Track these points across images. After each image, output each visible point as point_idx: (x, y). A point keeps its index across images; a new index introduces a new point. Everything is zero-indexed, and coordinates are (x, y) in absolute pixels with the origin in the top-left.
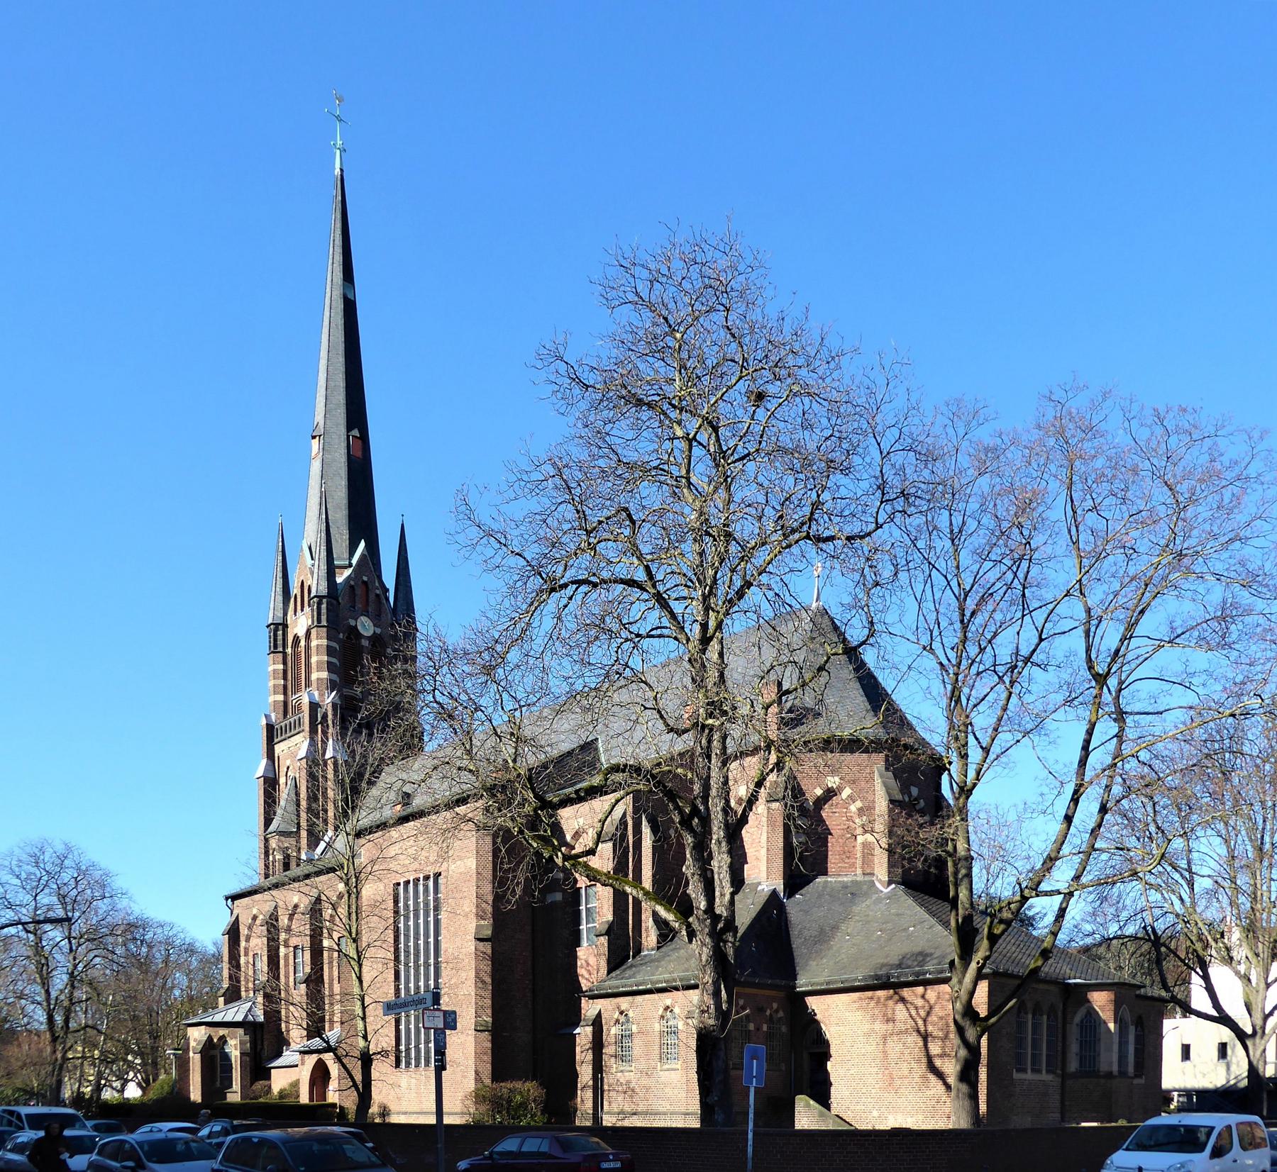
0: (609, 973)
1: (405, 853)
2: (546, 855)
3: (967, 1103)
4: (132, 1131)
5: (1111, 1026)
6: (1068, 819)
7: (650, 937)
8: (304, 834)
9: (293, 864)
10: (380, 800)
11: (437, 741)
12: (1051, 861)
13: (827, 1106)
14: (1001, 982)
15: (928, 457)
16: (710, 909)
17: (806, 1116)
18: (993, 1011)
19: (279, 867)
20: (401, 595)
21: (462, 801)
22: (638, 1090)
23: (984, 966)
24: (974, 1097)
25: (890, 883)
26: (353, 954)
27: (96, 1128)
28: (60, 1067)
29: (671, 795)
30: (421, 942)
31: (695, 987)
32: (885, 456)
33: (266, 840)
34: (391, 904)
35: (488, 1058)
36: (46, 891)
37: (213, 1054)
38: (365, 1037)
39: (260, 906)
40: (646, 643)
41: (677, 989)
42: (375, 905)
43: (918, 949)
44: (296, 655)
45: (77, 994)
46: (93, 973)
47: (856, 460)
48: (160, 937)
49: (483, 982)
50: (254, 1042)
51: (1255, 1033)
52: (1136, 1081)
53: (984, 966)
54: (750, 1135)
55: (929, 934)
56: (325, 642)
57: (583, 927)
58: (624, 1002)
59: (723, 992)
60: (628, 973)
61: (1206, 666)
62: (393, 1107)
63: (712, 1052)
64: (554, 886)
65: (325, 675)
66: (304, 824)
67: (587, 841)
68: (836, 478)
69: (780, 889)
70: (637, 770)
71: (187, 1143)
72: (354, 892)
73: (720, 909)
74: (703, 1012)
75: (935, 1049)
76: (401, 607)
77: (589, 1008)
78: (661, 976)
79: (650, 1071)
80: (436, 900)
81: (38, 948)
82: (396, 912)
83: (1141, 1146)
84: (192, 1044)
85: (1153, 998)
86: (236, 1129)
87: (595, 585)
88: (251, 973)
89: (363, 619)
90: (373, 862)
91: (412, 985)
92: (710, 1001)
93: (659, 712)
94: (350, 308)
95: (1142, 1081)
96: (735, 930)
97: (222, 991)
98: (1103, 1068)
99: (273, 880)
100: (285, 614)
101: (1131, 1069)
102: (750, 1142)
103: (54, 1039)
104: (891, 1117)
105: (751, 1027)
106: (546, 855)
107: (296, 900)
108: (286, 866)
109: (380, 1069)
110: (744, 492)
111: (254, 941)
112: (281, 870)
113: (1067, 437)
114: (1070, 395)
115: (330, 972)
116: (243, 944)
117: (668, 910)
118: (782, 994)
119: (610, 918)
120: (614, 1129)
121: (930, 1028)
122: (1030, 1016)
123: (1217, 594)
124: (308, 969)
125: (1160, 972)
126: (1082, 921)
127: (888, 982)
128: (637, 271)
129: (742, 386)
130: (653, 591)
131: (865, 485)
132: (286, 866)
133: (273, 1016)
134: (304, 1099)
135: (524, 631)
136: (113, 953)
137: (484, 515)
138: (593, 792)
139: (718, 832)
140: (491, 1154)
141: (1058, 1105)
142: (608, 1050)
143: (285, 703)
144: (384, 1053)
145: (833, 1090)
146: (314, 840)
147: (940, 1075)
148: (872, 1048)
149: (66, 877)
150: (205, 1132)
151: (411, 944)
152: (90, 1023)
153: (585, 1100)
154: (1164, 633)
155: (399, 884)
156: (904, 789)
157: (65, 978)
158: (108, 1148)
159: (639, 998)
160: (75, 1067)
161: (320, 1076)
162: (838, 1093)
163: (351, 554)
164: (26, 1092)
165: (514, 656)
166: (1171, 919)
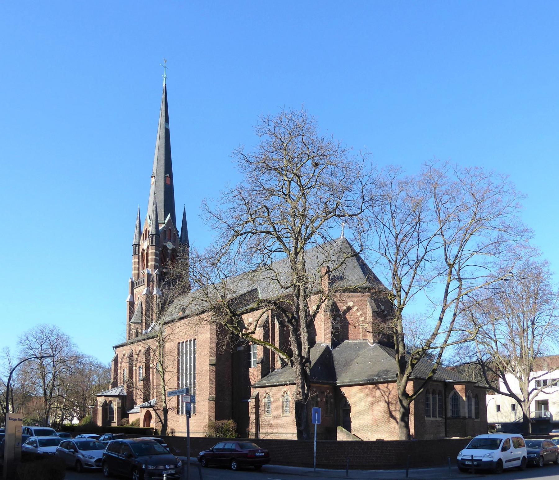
0: (262, 378)
1: (181, 332)
2: (236, 333)
3: (405, 429)
4: (74, 437)
5: (464, 398)
6: (441, 319)
7: (278, 364)
8: (144, 324)
9: (139, 335)
10: (173, 311)
11: (196, 288)
12: (435, 335)
13: (350, 431)
14: (420, 383)
15: (382, 186)
16: (300, 354)
17: (342, 435)
18: (415, 393)
19: (134, 335)
20: (183, 234)
21: (203, 312)
22: (273, 424)
23: (409, 376)
24: (407, 426)
25: (374, 343)
26: (161, 370)
27: (61, 436)
28: (48, 411)
29: (284, 311)
30: (188, 365)
31: (295, 384)
32: (363, 186)
33: (129, 326)
34: (177, 351)
35: (214, 411)
36: (46, 343)
37: (106, 407)
38: (165, 402)
39: (126, 351)
40: (274, 254)
41: (286, 385)
42: (171, 351)
43: (384, 369)
44: (143, 256)
45: (56, 383)
46: (61, 375)
47: (354, 186)
48: (88, 362)
49: (212, 381)
50: (122, 403)
51: (524, 401)
52: (475, 420)
53: (409, 376)
54: (315, 443)
55: (390, 363)
56: (154, 251)
57: (252, 360)
58: (268, 390)
59: (306, 386)
60: (269, 378)
61: (492, 260)
62: (176, 430)
63: (302, 411)
64: (239, 344)
65: (153, 263)
66: (144, 321)
67: (252, 328)
68: (347, 193)
69: (330, 345)
70: (269, 302)
71: (94, 443)
72: (162, 346)
73: (304, 354)
74: (297, 394)
75: (392, 408)
76: (183, 239)
77: (254, 392)
78: (282, 380)
79: (277, 416)
80: (194, 349)
81: (42, 365)
82: (179, 354)
83: (475, 447)
84: (99, 403)
85: (481, 387)
86: (114, 438)
87: (253, 233)
88: (122, 377)
89: (169, 242)
90: (169, 335)
91: (184, 382)
92: (300, 390)
93: (278, 280)
94: (167, 132)
95: (479, 420)
96: (310, 362)
97: (111, 383)
98: (462, 415)
99: (131, 341)
100: (139, 241)
101: (473, 415)
102: (315, 446)
103: (46, 400)
104: (376, 435)
105: (319, 399)
106: (236, 333)
107: (140, 348)
108: (137, 336)
109: (170, 415)
110: (310, 199)
111: (123, 364)
112: (135, 337)
113: (432, 181)
114: (433, 163)
115: (153, 377)
116: (119, 365)
117: (283, 354)
118: (331, 387)
119: (262, 356)
120: (263, 440)
121: (390, 400)
122: (431, 395)
123: (495, 233)
124: (144, 375)
125: (486, 377)
126: (450, 356)
127: (372, 382)
128: (270, 123)
129: (310, 162)
130: (276, 235)
131: (357, 195)
132: (137, 336)
133: (130, 394)
134: (142, 426)
135: (227, 251)
136: (70, 367)
137: (212, 209)
138: (253, 310)
139: (303, 325)
140: (213, 449)
141: (444, 430)
142: (261, 408)
143: (138, 274)
144: (172, 409)
145: (352, 424)
146: (148, 326)
147: (395, 418)
148: (367, 407)
149: (53, 338)
150: (102, 438)
151: (184, 366)
152: (60, 394)
153: (252, 428)
154: (475, 248)
155: (179, 343)
156: (378, 307)
157: (51, 376)
158: (64, 444)
159: (274, 388)
160: (54, 411)
161: (148, 417)
162: (354, 426)
163: (165, 219)
164: (34, 420)
165: (223, 259)
166: (488, 356)
